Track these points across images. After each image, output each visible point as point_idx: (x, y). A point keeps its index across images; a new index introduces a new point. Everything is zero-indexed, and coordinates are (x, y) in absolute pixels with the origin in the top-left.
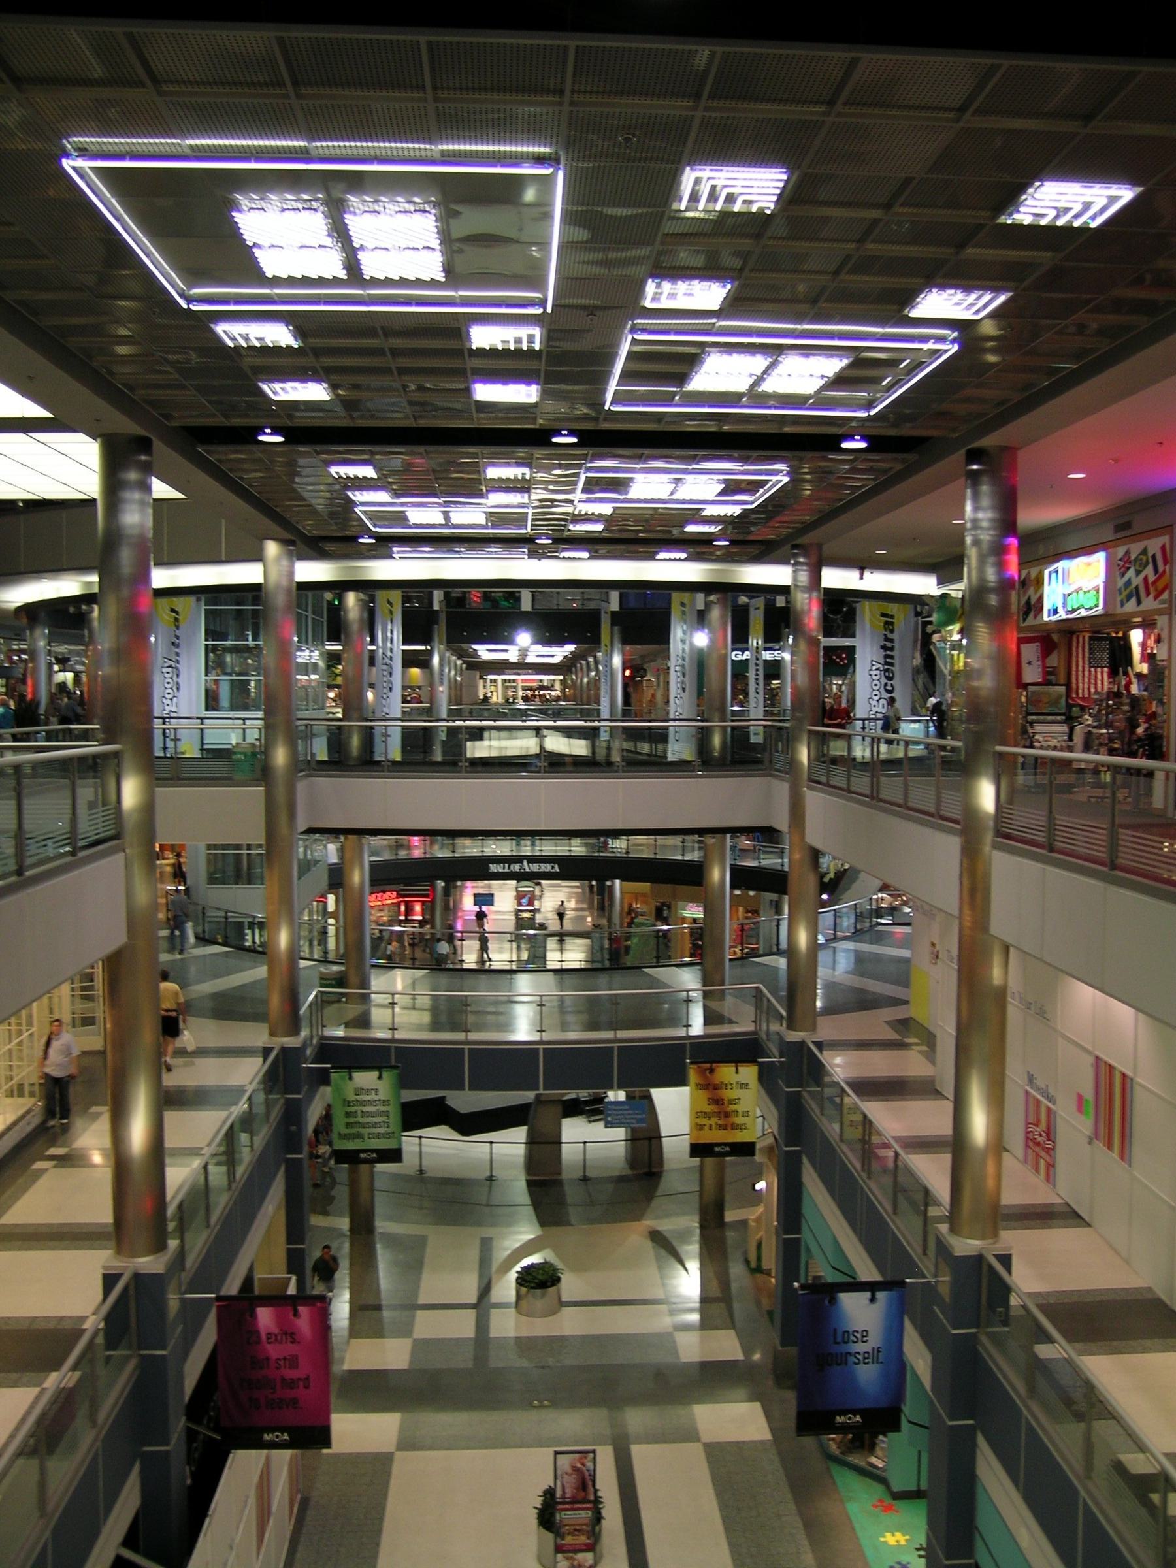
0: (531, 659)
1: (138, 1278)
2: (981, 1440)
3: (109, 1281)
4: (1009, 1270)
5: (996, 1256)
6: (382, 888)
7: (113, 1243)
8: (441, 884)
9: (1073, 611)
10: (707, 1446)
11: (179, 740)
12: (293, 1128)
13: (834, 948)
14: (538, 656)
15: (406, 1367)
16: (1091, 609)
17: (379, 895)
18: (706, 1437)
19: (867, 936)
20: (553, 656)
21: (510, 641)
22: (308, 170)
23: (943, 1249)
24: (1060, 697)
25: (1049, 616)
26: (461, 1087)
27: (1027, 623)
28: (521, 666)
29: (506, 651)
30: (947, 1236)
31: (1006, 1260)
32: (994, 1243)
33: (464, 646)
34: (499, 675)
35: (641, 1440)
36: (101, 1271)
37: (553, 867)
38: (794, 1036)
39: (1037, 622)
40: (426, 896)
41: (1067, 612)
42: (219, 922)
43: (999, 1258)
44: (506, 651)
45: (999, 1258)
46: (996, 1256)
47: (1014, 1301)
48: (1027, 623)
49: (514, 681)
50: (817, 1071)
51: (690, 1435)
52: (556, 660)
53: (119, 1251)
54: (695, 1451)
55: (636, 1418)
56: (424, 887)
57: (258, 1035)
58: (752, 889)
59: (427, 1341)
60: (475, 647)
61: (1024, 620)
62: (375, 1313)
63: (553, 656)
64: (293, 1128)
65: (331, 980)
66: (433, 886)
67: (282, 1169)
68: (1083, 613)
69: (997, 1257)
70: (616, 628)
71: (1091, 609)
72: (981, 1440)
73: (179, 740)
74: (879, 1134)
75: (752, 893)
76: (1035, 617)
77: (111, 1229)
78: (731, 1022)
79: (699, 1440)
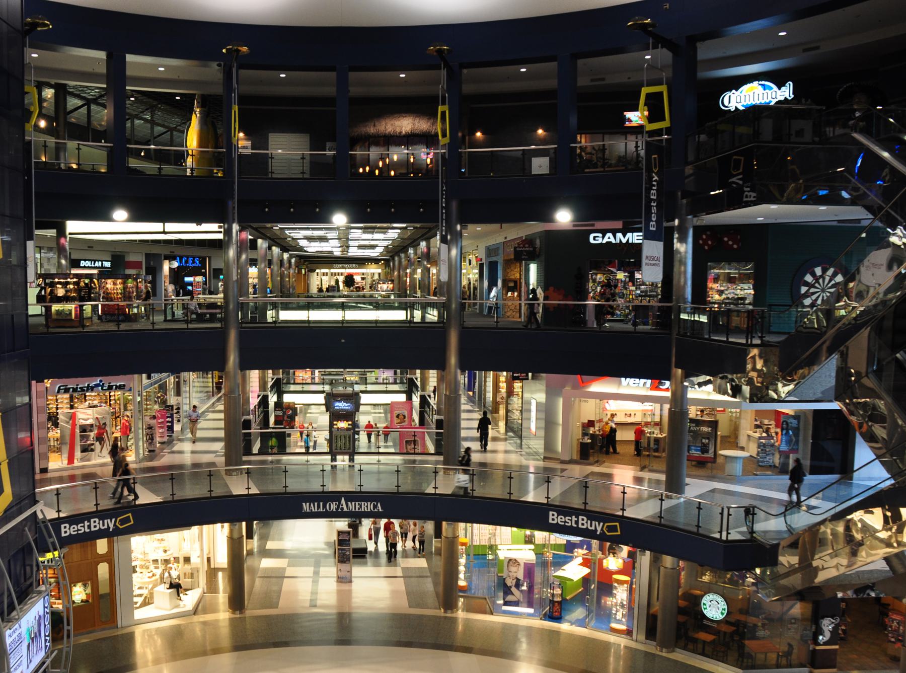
20: (373, 247)
37: (375, 507)
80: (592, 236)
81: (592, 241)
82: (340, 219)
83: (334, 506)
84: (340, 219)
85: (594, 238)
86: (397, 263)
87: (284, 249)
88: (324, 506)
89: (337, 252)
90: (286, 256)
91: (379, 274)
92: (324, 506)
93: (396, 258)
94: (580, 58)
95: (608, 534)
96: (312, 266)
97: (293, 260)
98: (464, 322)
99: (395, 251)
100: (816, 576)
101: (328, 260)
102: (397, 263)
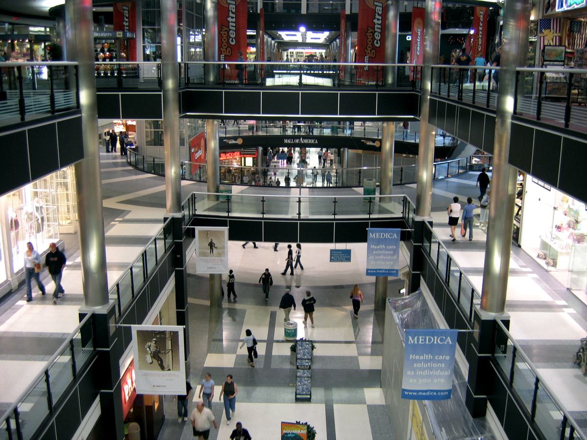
0: (309, 40)
1: (94, 316)
2: (489, 405)
3: (82, 316)
4: (508, 329)
5: (502, 321)
6: (233, 150)
7: (84, 302)
8: (260, 149)
9: (571, 5)
10: (368, 406)
11: (333, 202)
12: (179, 256)
13: (447, 181)
14: (312, 38)
15: (233, 366)
16: (579, 4)
17: (232, 154)
18: (368, 403)
19: (463, 176)
20: (319, 39)
21: (296, 29)
22: (568, 138)
23: (477, 316)
24: (562, 52)
25: (559, 8)
26: (261, 241)
27: (548, 14)
28: (304, 45)
29: (295, 35)
30: (479, 311)
31: (507, 323)
32: (501, 315)
33: (274, 32)
34: (295, 49)
35: (338, 402)
36: (78, 312)
37: (314, 141)
38: (418, 219)
39: (553, 12)
40: (255, 154)
41: (567, 7)
42: (151, 164)
43: (503, 321)
44: (295, 35)
45: (503, 321)
46: (502, 321)
47: (509, 343)
48: (548, 14)
49: (302, 53)
50: (429, 235)
51: (362, 402)
52: (321, 41)
53: (87, 303)
54: (364, 408)
55: (337, 394)
56: (253, 150)
57: (160, 214)
58: (411, 154)
59: (233, 353)
60: (280, 33)
61: (546, 12)
62: (220, 343)
63: (319, 39)
64: (179, 256)
65: (535, 374)
66: (257, 150)
67: (174, 274)
68: (576, 7)
69: (502, 321)
70: (348, 23)
71: (579, 4)
72: (489, 405)
73: (333, 202)
74: (457, 265)
75: (411, 156)
76: (552, 10)
77: (83, 297)
78: (392, 213)
79: (366, 403)
80: (407, 37)
81: (407, 39)
82: (302, 29)
83: (297, 141)
84: (302, 29)
85: (408, 38)
86: (332, 46)
87: (273, 39)
88: (294, 141)
89: (300, 40)
90: (273, 42)
91: (160, 64)
92: (294, 141)
93: (332, 44)
94: (356, 121)
95: (441, 343)
96: (285, 48)
97: (276, 44)
98: (195, 210)
99: (330, 40)
100: (481, 174)
101: (295, 44)
102: (332, 46)
